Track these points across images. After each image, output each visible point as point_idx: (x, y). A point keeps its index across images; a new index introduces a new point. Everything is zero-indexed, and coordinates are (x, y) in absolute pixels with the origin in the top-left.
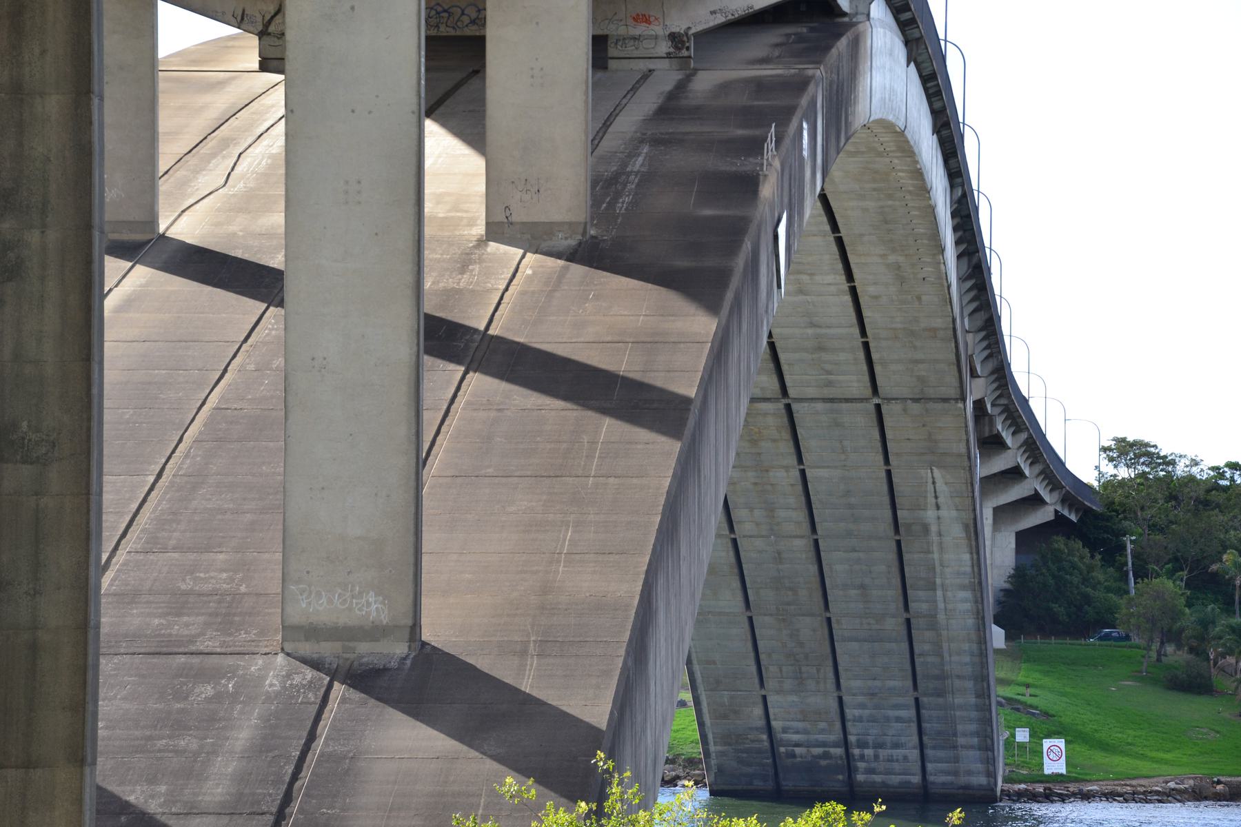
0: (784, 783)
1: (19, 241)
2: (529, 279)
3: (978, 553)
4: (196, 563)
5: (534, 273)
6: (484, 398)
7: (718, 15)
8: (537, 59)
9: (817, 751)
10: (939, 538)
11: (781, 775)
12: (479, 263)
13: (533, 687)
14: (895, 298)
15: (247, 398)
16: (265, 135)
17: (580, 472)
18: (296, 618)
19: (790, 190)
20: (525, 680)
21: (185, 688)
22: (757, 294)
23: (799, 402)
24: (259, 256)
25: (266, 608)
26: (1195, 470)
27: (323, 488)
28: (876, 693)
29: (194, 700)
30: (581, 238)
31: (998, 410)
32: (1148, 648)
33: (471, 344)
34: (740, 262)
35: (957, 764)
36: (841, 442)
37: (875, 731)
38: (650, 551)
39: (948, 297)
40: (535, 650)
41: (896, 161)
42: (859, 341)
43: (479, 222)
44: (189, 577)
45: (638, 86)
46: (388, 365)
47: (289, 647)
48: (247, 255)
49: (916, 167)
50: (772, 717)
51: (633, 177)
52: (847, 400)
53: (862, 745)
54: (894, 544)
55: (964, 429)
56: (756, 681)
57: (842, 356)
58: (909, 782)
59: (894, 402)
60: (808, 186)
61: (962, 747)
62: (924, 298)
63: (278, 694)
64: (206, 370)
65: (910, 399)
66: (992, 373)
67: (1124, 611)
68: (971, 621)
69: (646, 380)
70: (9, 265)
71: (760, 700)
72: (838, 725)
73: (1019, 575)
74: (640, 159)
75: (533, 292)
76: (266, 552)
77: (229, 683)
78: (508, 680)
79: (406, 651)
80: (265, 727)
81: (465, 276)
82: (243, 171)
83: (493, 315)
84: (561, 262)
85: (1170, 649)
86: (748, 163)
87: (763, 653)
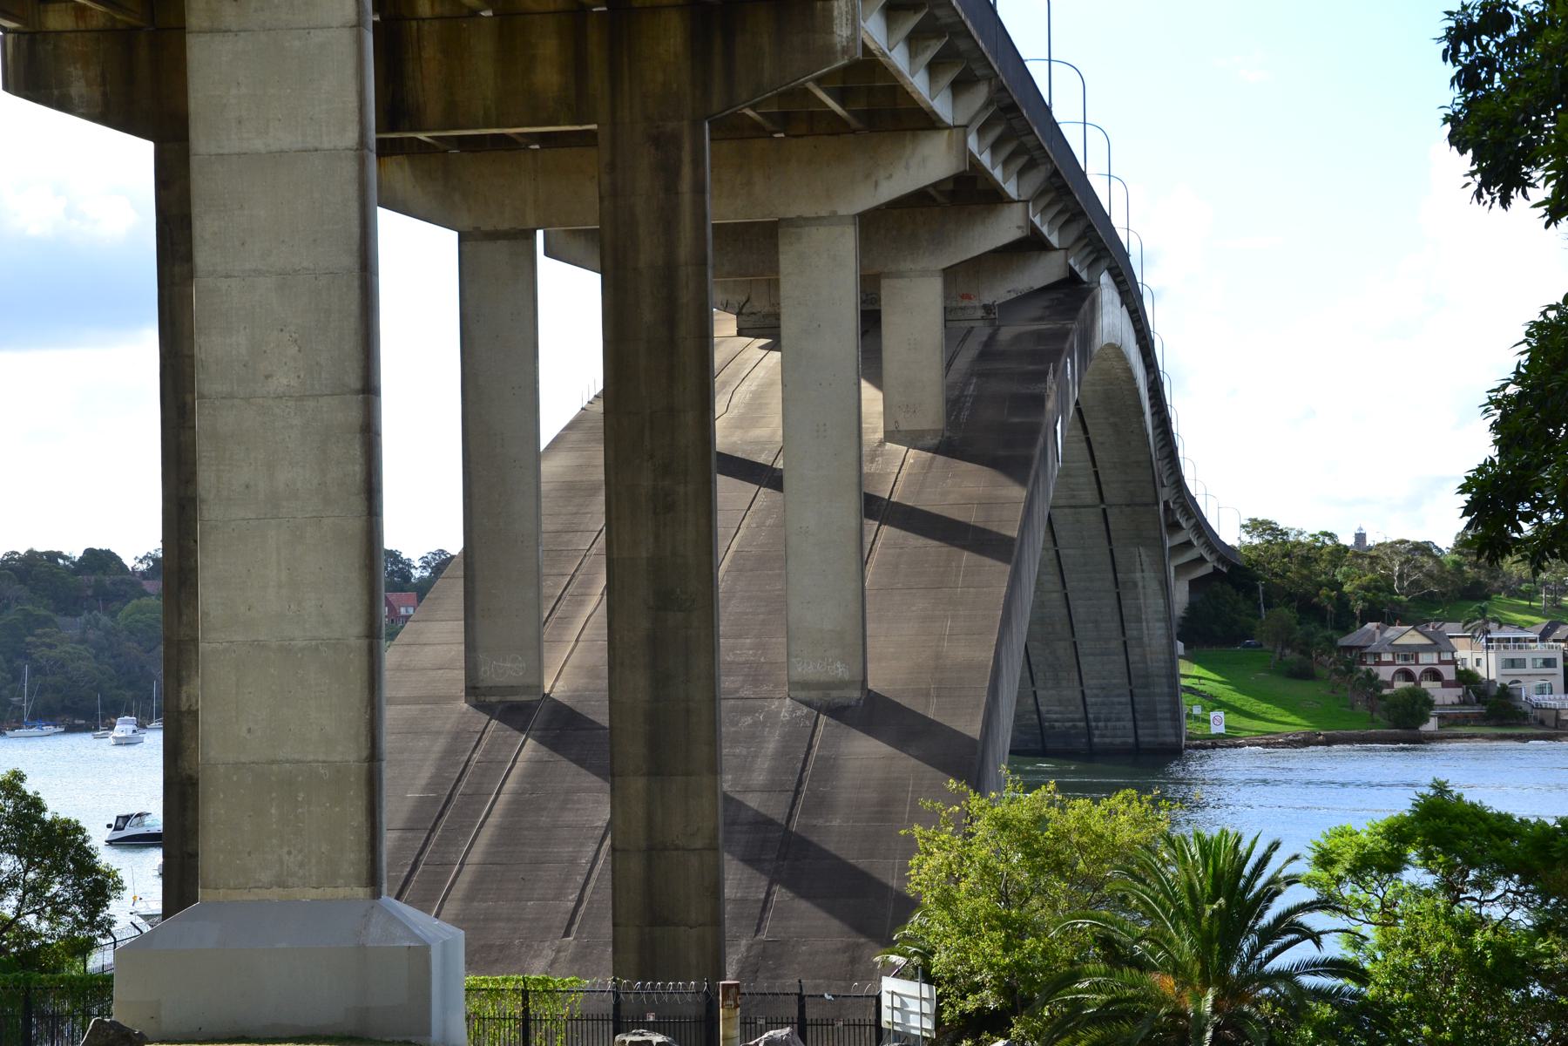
2: (913, 465)
3: (1168, 599)
5: (915, 462)
7: (1012, 293)
18: (795, 676)
26: (1302, 539)
31: (1177, 506)
32: (1274, 652)
34: (1037, 452)
42: (1091, 471)
52: (1085, 507)
53: (1097, 720)
54: (1115, 596)
56: (1030, 682)
63: (788, 722)
66: (1173, 484)
67: (1259, 629)
68: (1164, 641)
69: (987, 527)
71: (1031, 693)
72: (1082, 708)
73: (1192, 608)
74: (972, 387)
75: (915, 474)
83: (893, 488)
84: (930, 454)
85: (1288, 651)
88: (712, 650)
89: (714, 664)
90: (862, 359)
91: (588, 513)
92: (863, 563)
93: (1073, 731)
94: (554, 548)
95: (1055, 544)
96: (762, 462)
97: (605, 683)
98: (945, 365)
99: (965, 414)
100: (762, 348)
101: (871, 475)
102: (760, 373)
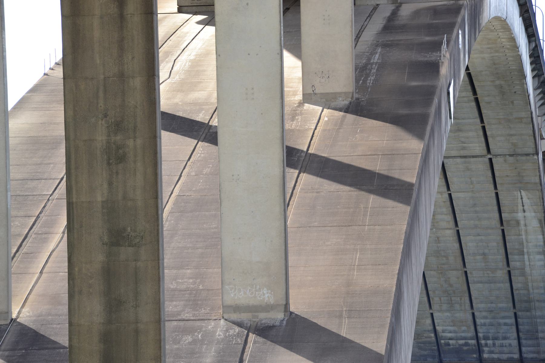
0: (444, 359)
1: (124, 145)
2: (327, 123)
4: (177, 275)
6: (310, 186)
8: (326, 11)
9: (462, 342)
10: (525, 227)
11: (442, 355)
12: (301, 115)
13: (347, 334)
14: (499, 103)
15: (193, 190)
16: (186, 49)
17: (361, 223)
19: (454, 68)
20: (343, 330)
21: (178, 337)
22: (441, 123)
23: (447, 158)
24: (190, 115)
25: (213, 297)
27: (240, 238)
28: (493, 311)
29: (183, 343)
30: (351, 100)
33: (300, 158)
34: (433, 110)
35: (539, 348)
36: (470, 178)
37: (493, 331)
38: (399, 263)
39: (528, 101)
40: (346, 315)
41: (500, 34)
42: (479, 126)
43: (298, 93)
44: (174, 282)
45: (371, 14)
46: (269, 178)
47: (226, 316)
48: (184, 115)
49: (512, 36)
50: (436, 324)
51: (374, 65)
52: (473, 157)
53: (486, 338)
54: (500, 232)
55: (538, 169)
56: (427, 305)
57: (471, 134)
58: (513, 358)
59: (499, 156)
60: (462, 63)
61: (541, 338)
62: (515, 102)
63: (223, 340)
64: (171, 176)
65: (508, 155)
69: (390, 175)
70: (120, 156)
71: (429, 316)
72: (472, 328)
74: (377, 56)
75: (329, 130)
76: (210, 268)
77: (199, 335)
78: (334, 330)
79: (283, 316)
80: (218, 356)
81: (294, 122)
82: (177, 69)
84: (342, 113)
86: (433, 56)
87: (431, 291)
88: (158, 279)
89: (159, 292)
90: (284, 32)
91: (50, 164)
92: (286, 205)
93: (465, 348)
94: (22, 194)
95: (448, 188)
96: (199, 120)
97: (64, 309)
98: (354, 38)
99: (371, 80)
100: (199, 23)
101: (292, 131)
102: (197, 45)
